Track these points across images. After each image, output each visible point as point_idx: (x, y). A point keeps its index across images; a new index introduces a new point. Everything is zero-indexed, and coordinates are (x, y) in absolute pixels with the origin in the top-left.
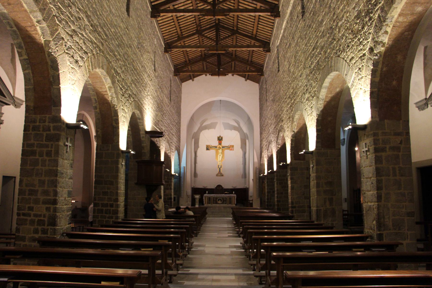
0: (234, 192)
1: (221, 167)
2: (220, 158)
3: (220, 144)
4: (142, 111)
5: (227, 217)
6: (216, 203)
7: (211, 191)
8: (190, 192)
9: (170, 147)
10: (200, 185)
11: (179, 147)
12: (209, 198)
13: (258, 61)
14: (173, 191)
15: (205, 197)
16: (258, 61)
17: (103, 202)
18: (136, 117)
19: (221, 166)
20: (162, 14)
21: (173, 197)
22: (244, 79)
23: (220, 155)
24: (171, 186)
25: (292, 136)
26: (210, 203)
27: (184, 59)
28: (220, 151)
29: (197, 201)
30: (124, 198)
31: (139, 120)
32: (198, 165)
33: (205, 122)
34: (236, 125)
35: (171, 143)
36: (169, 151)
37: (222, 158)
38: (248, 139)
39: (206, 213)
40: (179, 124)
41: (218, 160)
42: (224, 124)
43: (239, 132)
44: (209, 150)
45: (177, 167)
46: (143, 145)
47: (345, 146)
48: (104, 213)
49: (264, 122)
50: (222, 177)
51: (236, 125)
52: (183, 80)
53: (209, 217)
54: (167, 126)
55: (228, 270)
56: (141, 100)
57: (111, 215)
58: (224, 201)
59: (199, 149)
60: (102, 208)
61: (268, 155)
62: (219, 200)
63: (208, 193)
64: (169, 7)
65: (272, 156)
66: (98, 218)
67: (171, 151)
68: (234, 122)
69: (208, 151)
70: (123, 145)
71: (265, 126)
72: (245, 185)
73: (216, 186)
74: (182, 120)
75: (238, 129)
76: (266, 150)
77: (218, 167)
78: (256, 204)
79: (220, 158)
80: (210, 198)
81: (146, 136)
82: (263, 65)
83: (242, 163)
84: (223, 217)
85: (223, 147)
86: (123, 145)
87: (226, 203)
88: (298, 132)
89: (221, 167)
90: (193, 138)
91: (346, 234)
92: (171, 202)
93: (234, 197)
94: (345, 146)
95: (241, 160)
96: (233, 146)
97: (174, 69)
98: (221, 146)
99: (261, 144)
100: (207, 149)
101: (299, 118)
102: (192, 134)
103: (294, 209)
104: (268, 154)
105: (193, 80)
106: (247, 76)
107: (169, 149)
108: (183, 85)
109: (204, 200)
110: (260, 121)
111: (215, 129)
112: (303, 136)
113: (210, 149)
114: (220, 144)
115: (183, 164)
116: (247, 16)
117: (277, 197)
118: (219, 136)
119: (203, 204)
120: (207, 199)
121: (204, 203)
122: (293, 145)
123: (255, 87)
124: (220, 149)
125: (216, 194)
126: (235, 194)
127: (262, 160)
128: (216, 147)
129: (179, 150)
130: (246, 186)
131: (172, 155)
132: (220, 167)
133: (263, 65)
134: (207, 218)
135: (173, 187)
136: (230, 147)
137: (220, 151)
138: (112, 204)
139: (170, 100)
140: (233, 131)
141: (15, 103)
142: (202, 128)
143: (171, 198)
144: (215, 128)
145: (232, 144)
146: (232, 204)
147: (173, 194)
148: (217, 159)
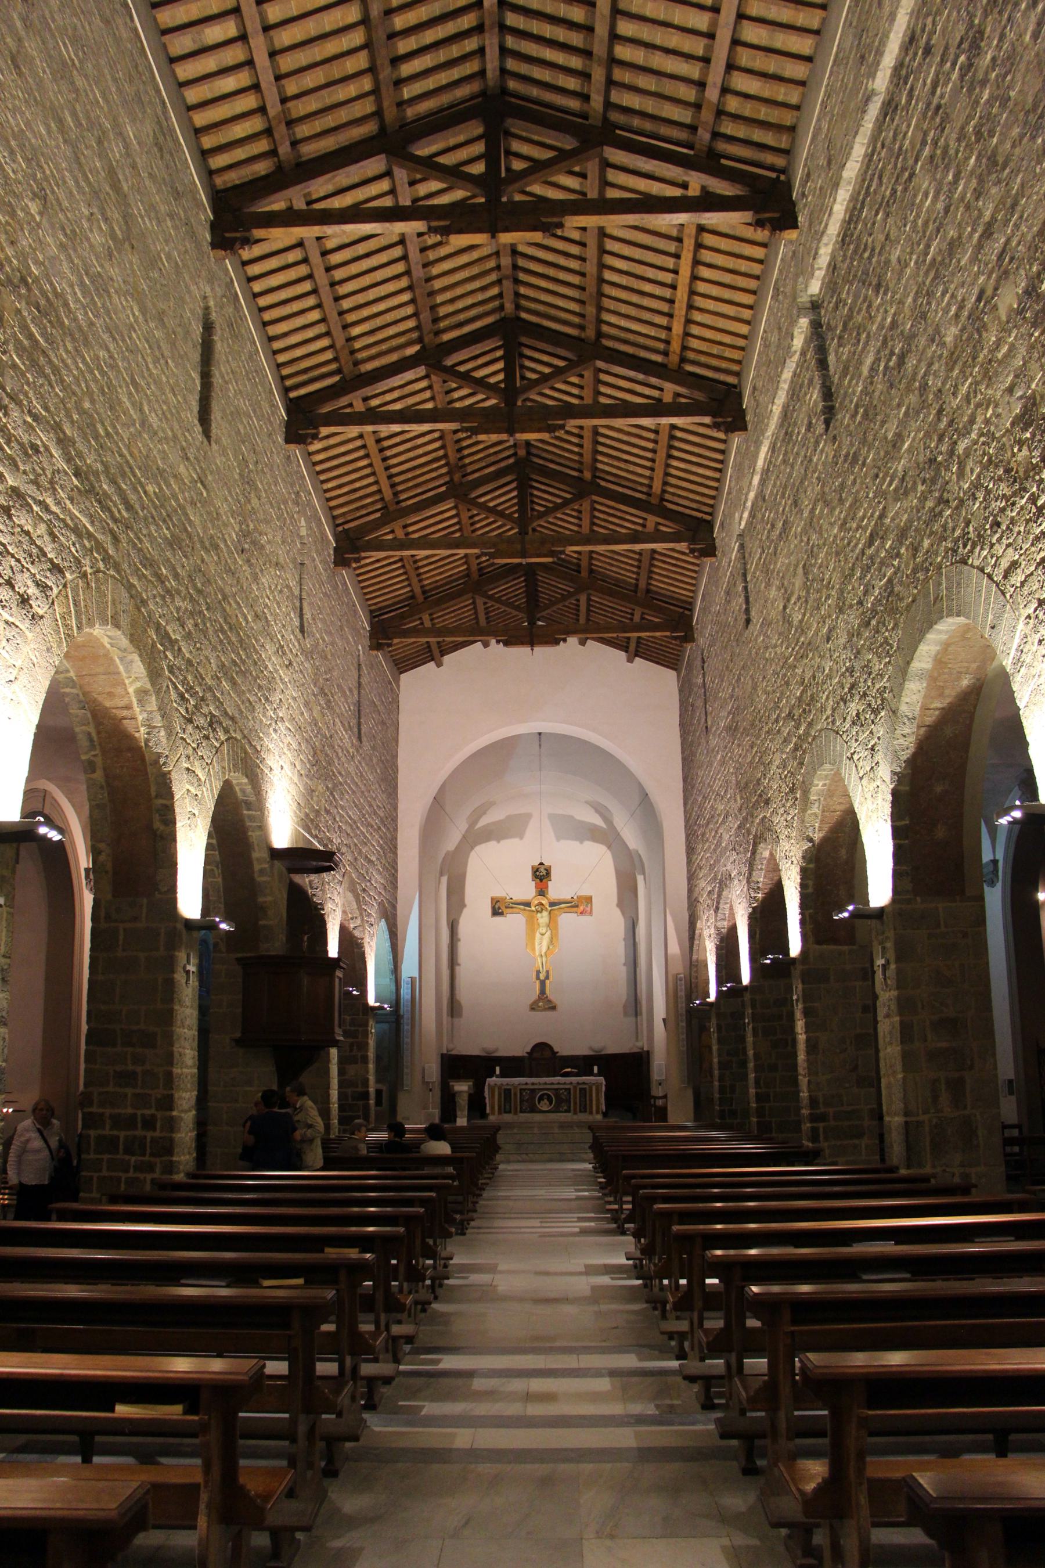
1: (547, 977)
2: (542, 944)
3: (542, 892)
6: (533, 1110)
7: (512, 1066)
8: (433, 1070)
9: (360, 908)
10: (469, 1046)
12: (507, 1093)
14: (371, 1066)
15: (492, 1089)
17: (117, 1111)
18: (236, 797)
19: (548, 972)
20: (363, 554)
21: (372, 1090)
22: (623, 655)
24: (367, 1051)
25: (803, 857)
26: (510, 1112)
28: (543, 918)
29: (463, 1102)
30: (196, 1093)
31: (249, 809)
32: (463, 972)
34: (598, 821)
35: (364, 890)
36: (358, 922)
37: (551, 941)
39: (497, 1149)
42: (552, 817)
43: (609, 847)
44: (502, 914)
45: (388, 981)
46: (261, 899)
47: (999, 885)
48: (121, 1151)
50: (549, 1013)
51: (598, 821)
52: (404, 664)
53: (508, 1162)
54: (349, 831)
56: (252, 736)
57: (147, 1158)
58: (561, 1100)
59: (466, 912)
60: (115, 1133)
61: (717, 929)
62: (541, 1099)
63: (503, 1075)
64: (351, 405)
66: (100, 1170)
67: (362, 920)
69: (498, 919)
71: (703, 822)
73: (528, 1049)
74: (401, 807)
75: (608, 837)
76: (712, 912)
77: (538, 978)
79: (542, 944)
81: (272, 866)
82: (691, 604)
83: (623, 960)
85: (552, 904)
87: (568, 1111)
88: (825, 840)
89: (547, 977)
90: (441, 874)
92: (367, 1107)
93: (598, 1086)
94: (999, 885)
96: (589, 900)
98: (545, 902)
100: (496, 912)
102: (440, 861)
103: (821, 1125)
104: (719, 924)
106: (633, 646)
107: (357, 913)
108: (402, 683)
109: (487, 1100)
110: (685, 804)
111: (521, 838)
112: (843, 853)
113: (505, 911)
114: (542, 892)
115: (409, 968)
116: (626, 429)
118: (536, 863)
119: (484, 1115)
120: (500, 1094)
121: (488, 1111)
122: (810, 890)
126: (599, 1074)
127: (695, 948)
128: (528, 904)
129: (395, 916)
130: (639, 1044)
132: (542, 977)
133: (691, 604)
135: (371, 1054)
136: (580, 905)
137: (543, 918)
138: (153, 1116)
139: (360, 738)
140: (588, 844)
142: (474, 838)
143: (366, 1095)
145: (585, 892)
146: (591, 1113)
147: (372, 1078)
148: (534, 949)
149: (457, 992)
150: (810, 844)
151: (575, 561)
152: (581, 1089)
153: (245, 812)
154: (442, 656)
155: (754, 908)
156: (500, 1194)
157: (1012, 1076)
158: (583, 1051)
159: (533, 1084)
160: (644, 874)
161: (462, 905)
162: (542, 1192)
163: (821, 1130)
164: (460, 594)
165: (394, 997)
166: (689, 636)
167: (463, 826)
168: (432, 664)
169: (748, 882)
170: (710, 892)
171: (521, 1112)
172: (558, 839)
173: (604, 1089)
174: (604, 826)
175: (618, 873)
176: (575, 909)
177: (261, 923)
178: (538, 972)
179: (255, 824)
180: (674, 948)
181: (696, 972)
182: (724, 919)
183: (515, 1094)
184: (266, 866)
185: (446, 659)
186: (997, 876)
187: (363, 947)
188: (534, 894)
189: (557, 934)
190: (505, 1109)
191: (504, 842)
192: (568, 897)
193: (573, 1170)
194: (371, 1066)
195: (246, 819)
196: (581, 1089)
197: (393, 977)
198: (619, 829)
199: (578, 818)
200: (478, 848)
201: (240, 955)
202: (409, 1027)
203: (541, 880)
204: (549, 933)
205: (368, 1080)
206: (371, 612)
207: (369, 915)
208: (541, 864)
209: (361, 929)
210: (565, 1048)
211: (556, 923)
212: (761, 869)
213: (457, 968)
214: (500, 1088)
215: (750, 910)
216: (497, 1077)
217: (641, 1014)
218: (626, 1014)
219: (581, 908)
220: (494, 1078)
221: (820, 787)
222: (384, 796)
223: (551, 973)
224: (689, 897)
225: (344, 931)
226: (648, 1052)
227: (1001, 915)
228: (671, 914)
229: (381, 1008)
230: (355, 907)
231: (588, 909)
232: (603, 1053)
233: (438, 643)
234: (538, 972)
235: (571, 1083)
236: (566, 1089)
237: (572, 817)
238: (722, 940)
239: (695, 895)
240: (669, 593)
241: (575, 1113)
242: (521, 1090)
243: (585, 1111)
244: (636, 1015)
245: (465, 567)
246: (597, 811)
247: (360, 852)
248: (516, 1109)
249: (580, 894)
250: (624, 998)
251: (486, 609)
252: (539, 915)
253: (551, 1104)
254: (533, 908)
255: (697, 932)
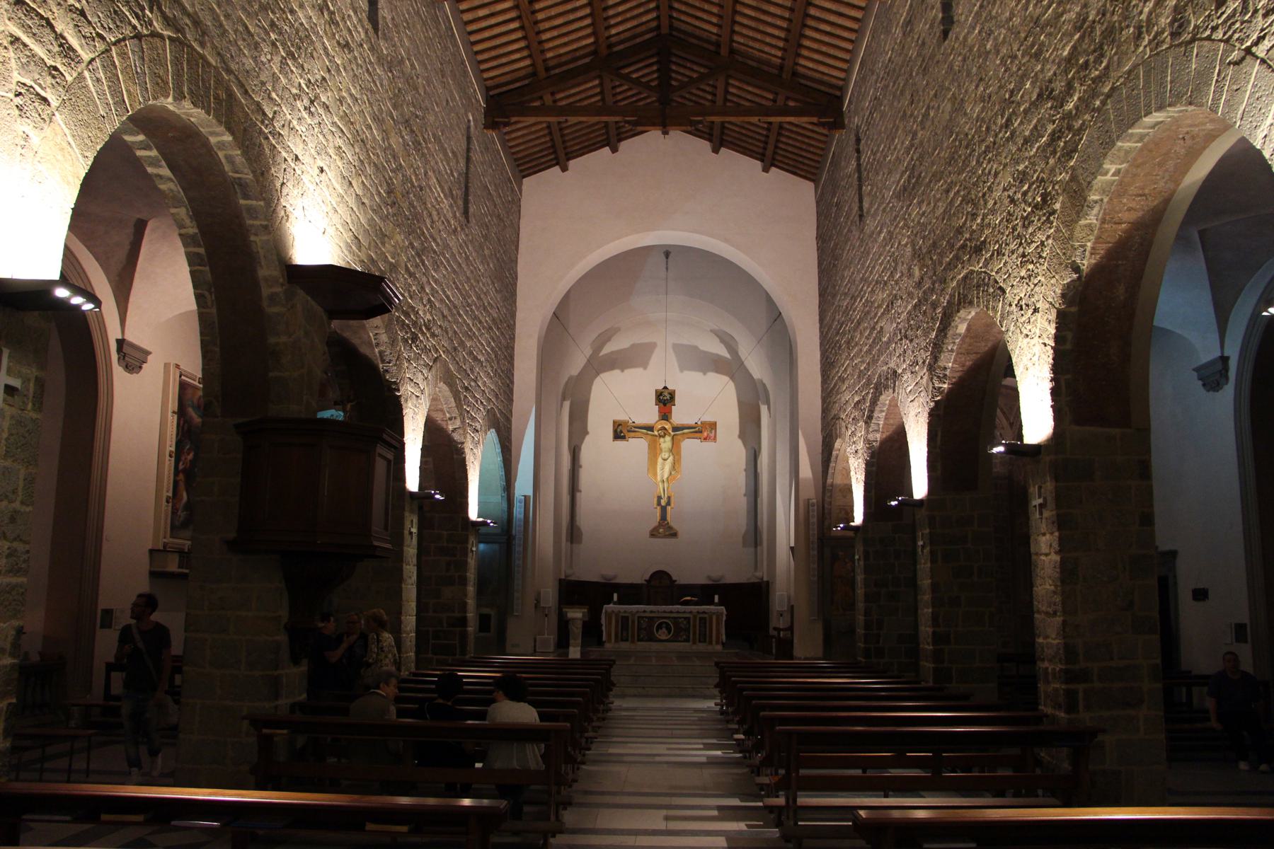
0: (716, 598)
1: (668, 503)
2: (663, 469)
3: (665, 416)
4: (261, 153)
5: (693, 696)
6: (652, 638)
7: (631, 593)
8: (550, 595)
9: (459, 406)
10: (588, 572)
11: (509, 420)
12: (624, 621)
13: (822, 68)
14: (471, 589)
15: (609, 616)
16: (822, 68)
18: (223, 173)
19: (669, 498)
21: (471, 615)
22: (758, 164)
23: (665, 460)
24: (466, 571)
25: (1063, 296)
26: (627, 640)
27: (528, 62)
28: (666, 443)
29: (576, 630)
31: (246, 197)
32: (583, 498)
33: (609, 339)
34: (722, 351)
35: (466, 389)
36: (458, 423)
37: (674, 467)
38: (768, 403)
39: (610, 685)
40: (505, 327)
41: (659, 478)
42: (676, 347)
43: (732, 378)
44: (623, 438)
45: (497, 499)
46: (272, 340)
47: (1229, 390)
49: (846, 312)
50: (673, 540)
51: (722, 351)
52: (528, 165)
53: (623, 696)
54: (446, 312)
55: (674, 798)
56: (252, 84)
58: (680, 630)
59: (588, 439)
61: (867, 441)
62: (659, 627)
63: (620, 602)
65: (897, 442)
67: (463, 422)
68: (717, 340)
69: (619, 443)
70: (412, 482)
71: (851, 325)
72: (756, 568)
73: (647, 577)
74: (520, 315)
75: (732, 367)
76: (861, 423)
77: (659, 504)
78: (807, 646)
79: (663, 469)
80: (625, 619)
82: (840, 89)
83: (743, 491)
84: (681, 696)
85: (675, 429)
86: (412, 482)
87: (687, 640)
88: (1097, 270)
89: (668, 503)
90: (564, 399)
91: (992, 711)
92: (464, 636)
93: (719, 615)
94: (1229, 390)
95: (741, 479)
96: (713, 426)
97: (487, 102)
98: (668, 426)
99: (825, 410)
100: (618, 436)
101: (1121, 183)
102: (562, 386)
103: (1081, 687)
104: (871, 437)
105: (564, 169)
107: (456, 413)
108: (524, 188)
109: (604, 628)
110: (821, 320)
111: (645, 368)
112: (1121, 291)
113: (628, 435)
114: (665, 416)
115: (523, 485)
117: (935, 618)
118: (660, 387)
119: (600, 643)
120: (617, 622)
121: (604, 638)
122: (1068, 346)
123: (804, 191)
124: (664, 437)
125: (648, 604)
126: (720, 604)
127: (831, 471)
128: (650, 428)
129: (509, 430)
130: (759, 574)
131: (469, 439)
132: (663, 503)
133: (840, 89)
134: (617, 703)
135: (471, 575)
136: (704, 431)
137: (666, 443)
139: (466, 212)
140: (712, 376)
141: (126, 358)
142: (599, 364)
143: (463, 621)
144: (644, 365)
145: (708, 418)
146: (711, 643)
147: (471, 602)
148: (655, 474)
149: (577, 518)
150: (1075, 276)
151: (714, 38)
152: (701, 619)
153: (242, 202)
154: (569, 159)
155: (936, 402)
156: (611, 751)
157: (1244, 618)
158: (702, 580)
159: (651, 612)
160: (768, 403)
161: (585, 432)
162: (661, 749)
163: (1081, 695)
164: (586, 69)
165: (505, 516)
166: (837, 122)
167: (588, 352)
168: (557, 168)
169: (931, 369)
170: (858, 402)
171: (639, 640)
172: (682, 369)
173: (724, 618)
174: (728, 356)
175: (741, 404)
176: (698, 435)
177: (271, 374)
178: (659, 498)
179: (257, 223)
180: (806, 471)
181: (831, 496)
182: (877, 431)
183: (633, 622)
184: (278, 289)
185: (572, 163)
186: (1227, 379)
187: (464, 453)
188: (657, 418)
189: (679, 460)
190: (622, 637)
191: (628, 372)
192: (691, 422)
193: (696, 710)
194: (471, 589)
195: (245, 214)
196: (701, 619)
197: (505, 495)
198: (743, 358)
199: (702, 348)
200: (602, 375)
201: (240, 420)
202: (521, 549)
203: (665, 405)
204: (671, 458)
205: (465, 604)
206: (488, 89)
207: (473, 419)
208: (665, 388)
209: (461, 431)
210: (685, 575)
211: (679, 447)
212: (952, 351)
213: (578, 494)
214: (617, 615)
215: (932, 404)
216: (615, 603)
217: (761, 544)
218: (745, 544)
219: (705, 434)
220: (611, 605)
221: (1108, 177)
222: (499, 296)
223: (672, 500)
224: (823, 418)
225: (433, 432)
226: (768, 582)
227: (1232, 424)
228: (803, 433)
229: (484, 524)
230: (453, 404)
231: (712, 435)
232: (721, 582)
233: (559, 123)
234: (659, 498)
235: (691, 612)
236: (685, 618)
237: (696, 348)
238: (872, 455)
239: (834, 412)
240: (817, 76)
241: (694, 643)
242: (639, 617)
243: (705, 641)
244: (756, 546)
245: (591, 40)
246: (722, 341)
247: (462, 343)
248: (633, 636)
249: (704, 419)
250: (743, 529)
251: (618, 135)
252: (662, 440)
253: (669, 633)
254: (656, 433)
255: (834, 453)
